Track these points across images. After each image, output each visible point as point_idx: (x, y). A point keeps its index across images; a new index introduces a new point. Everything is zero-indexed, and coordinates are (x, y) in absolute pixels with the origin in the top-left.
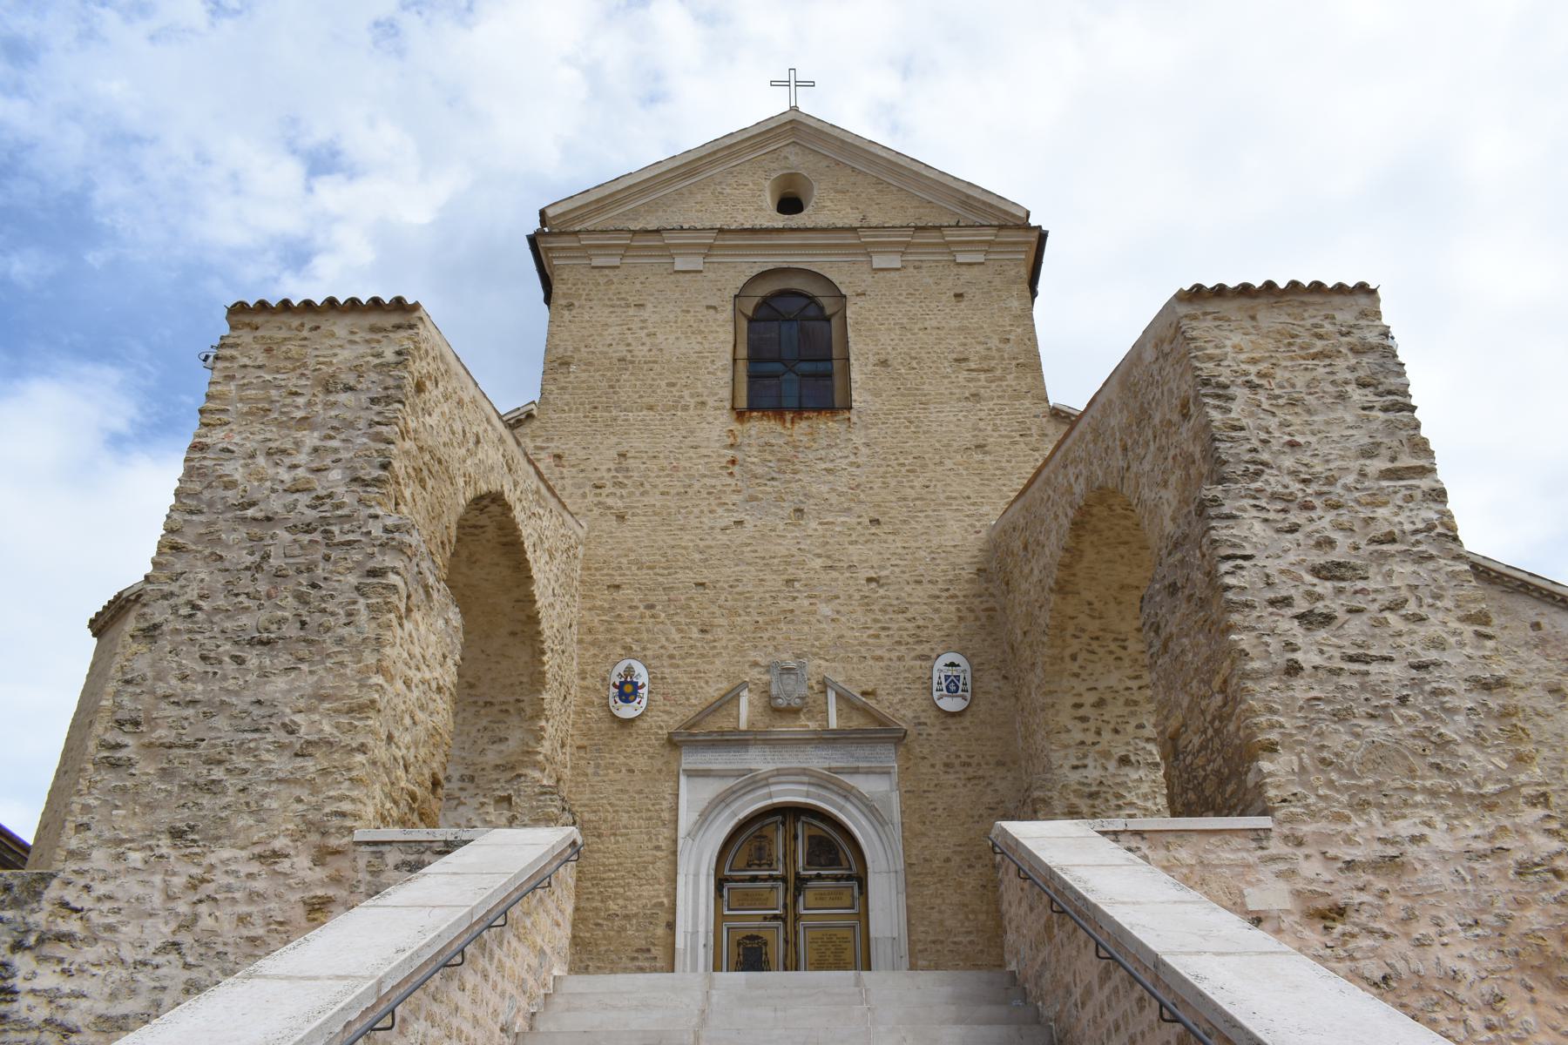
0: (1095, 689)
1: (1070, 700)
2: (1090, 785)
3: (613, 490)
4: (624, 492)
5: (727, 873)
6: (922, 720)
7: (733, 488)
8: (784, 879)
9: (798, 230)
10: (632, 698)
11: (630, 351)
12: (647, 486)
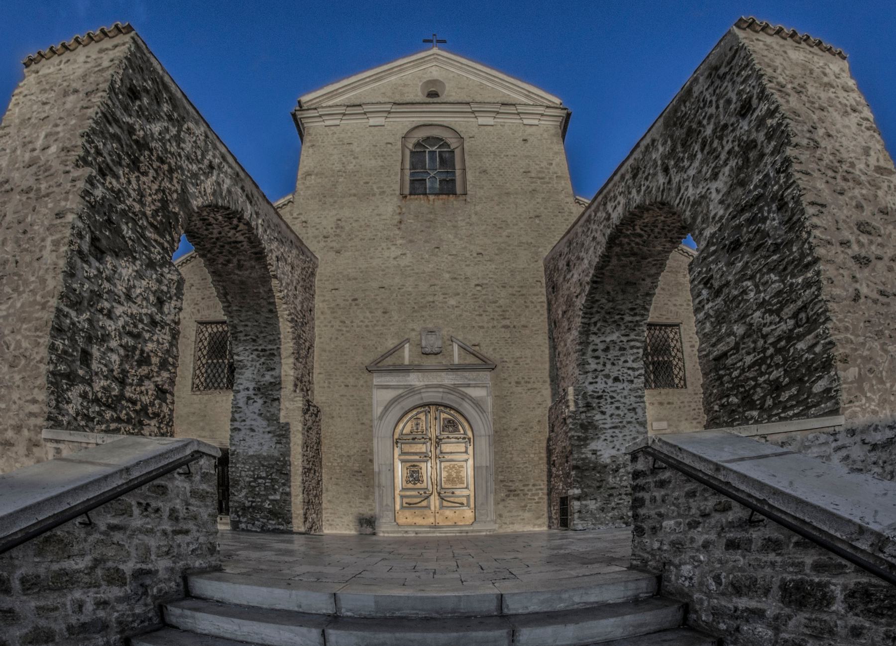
9: (437, 103)
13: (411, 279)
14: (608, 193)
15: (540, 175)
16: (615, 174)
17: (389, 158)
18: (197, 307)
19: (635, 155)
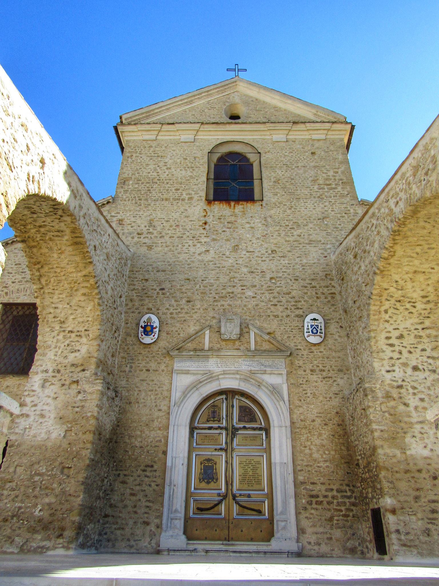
0: (398, 329)
1: (384, 335)
2: (397, 381)
3: (147, 236)
4: (152, 236)
5: (196, 425)
6: (299, 347)
7: (205, 235)
8: (226, 429)
10: (150, 333)
11: (158, 175)
12: (163, 234)
13: (213, 272)
14: (388, 193)
15: (328, 182)
16: (395, 174)
17: (197, 170)
18: (6, 290)
19: (415, 154)
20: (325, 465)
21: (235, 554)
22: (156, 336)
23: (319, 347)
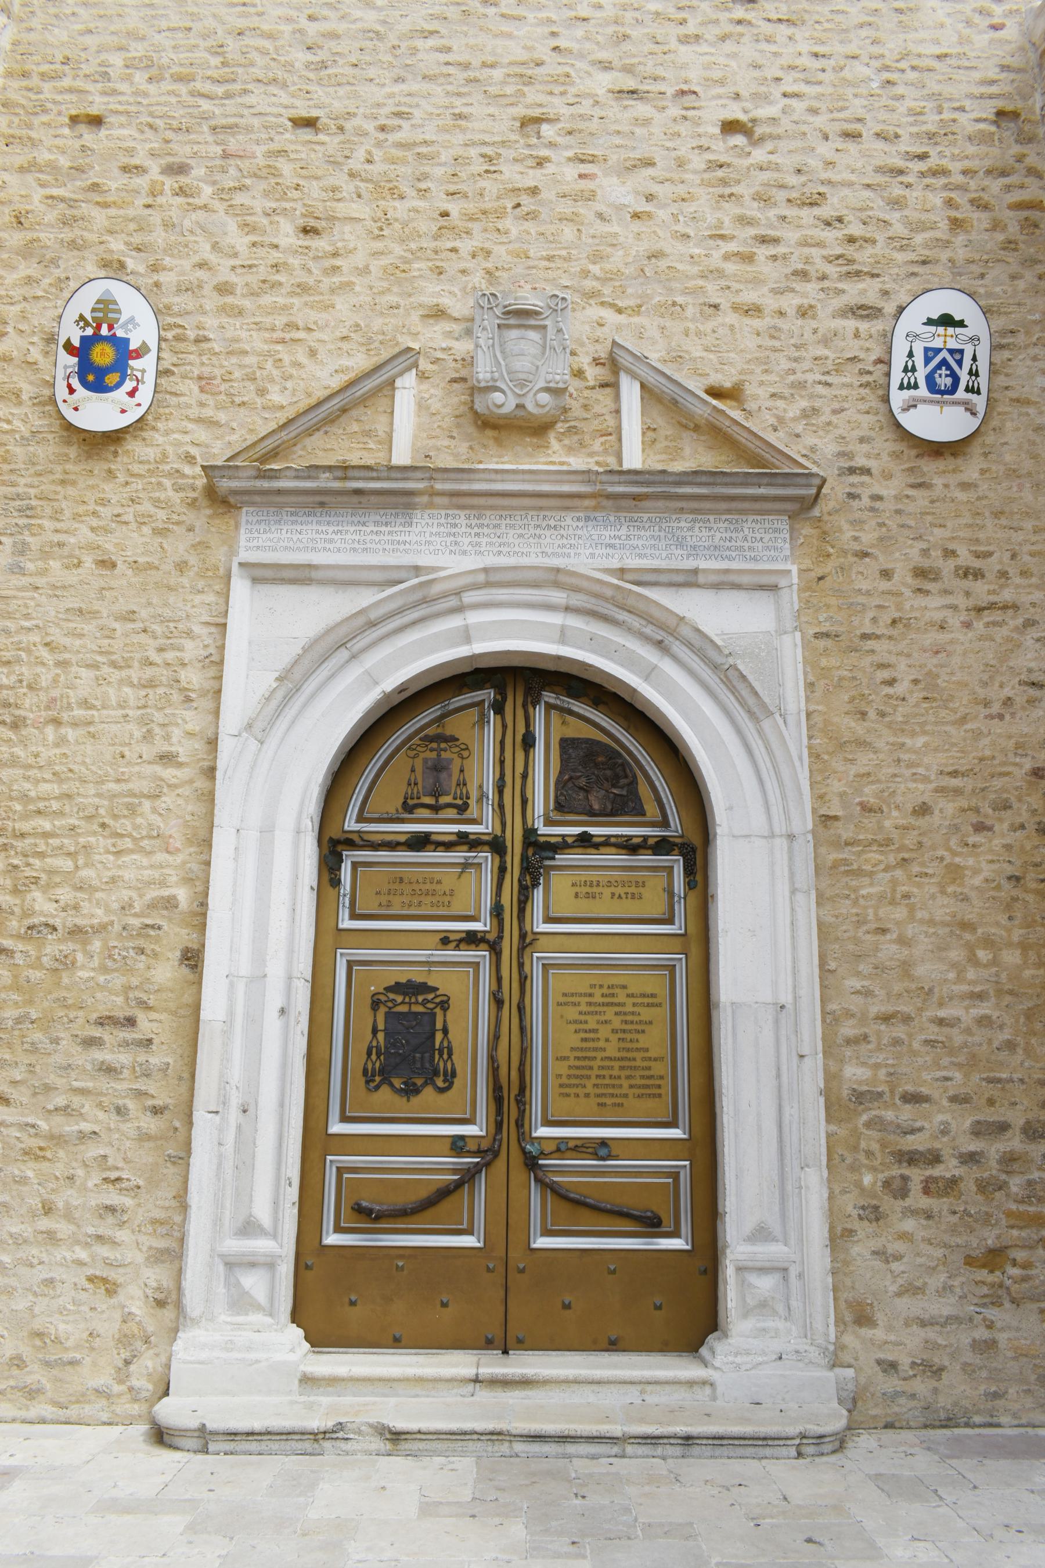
6: (860, 461)
8: (497, 846)
10: (112, 379)
20: (975, 1012)
21: (536, 1448)
22: (145, 394)
23: (959, 461)
